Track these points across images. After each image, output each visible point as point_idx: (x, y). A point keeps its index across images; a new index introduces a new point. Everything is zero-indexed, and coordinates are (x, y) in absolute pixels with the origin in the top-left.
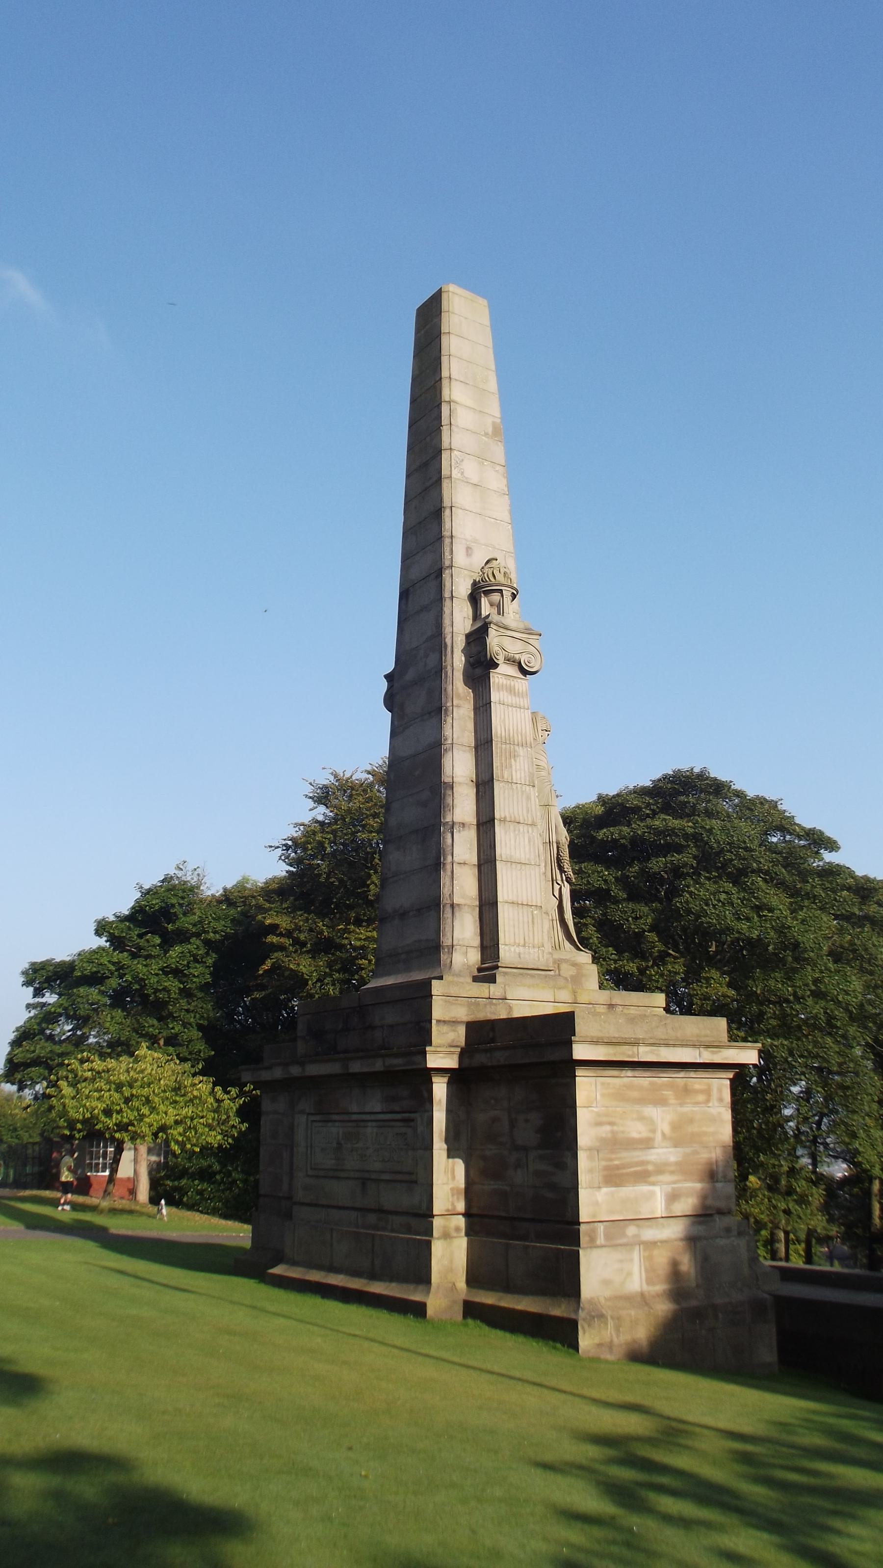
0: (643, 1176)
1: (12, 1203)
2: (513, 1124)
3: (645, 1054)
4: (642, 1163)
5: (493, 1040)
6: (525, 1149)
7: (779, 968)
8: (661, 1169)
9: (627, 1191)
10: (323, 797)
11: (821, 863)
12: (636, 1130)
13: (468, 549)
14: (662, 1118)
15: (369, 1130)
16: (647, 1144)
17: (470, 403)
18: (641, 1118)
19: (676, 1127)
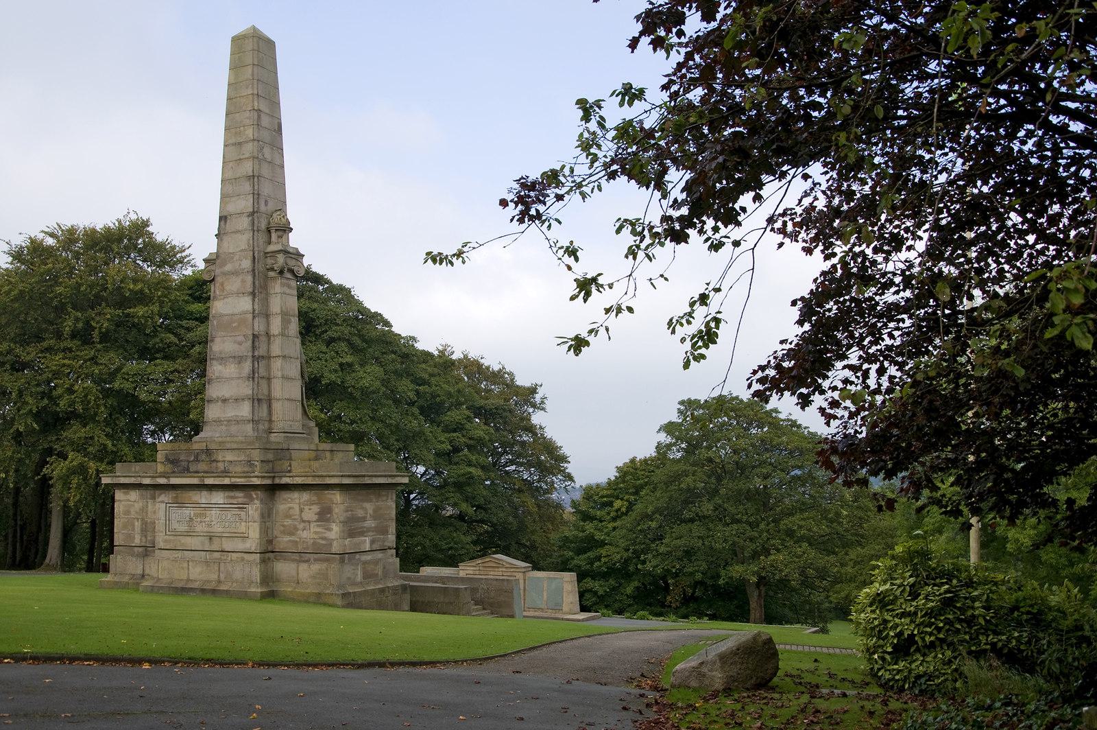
0: (362, 534)
1: (18, 559)
2: (301, 511)
3: (368, 481)
4: (318, 526)
5: (290, 471)
6: (309, 522)
7: (62, 323)
8: (369, 530)
9: (356, 540)
10: (17, 255)
11: (188, 272)
12: (360, 513)
13: (266, 202)
14: (369, 507)
15: (213, 512)
16: (364, 519)
17: (267, 111)
18: (362, 508)
19: (375, 511)
